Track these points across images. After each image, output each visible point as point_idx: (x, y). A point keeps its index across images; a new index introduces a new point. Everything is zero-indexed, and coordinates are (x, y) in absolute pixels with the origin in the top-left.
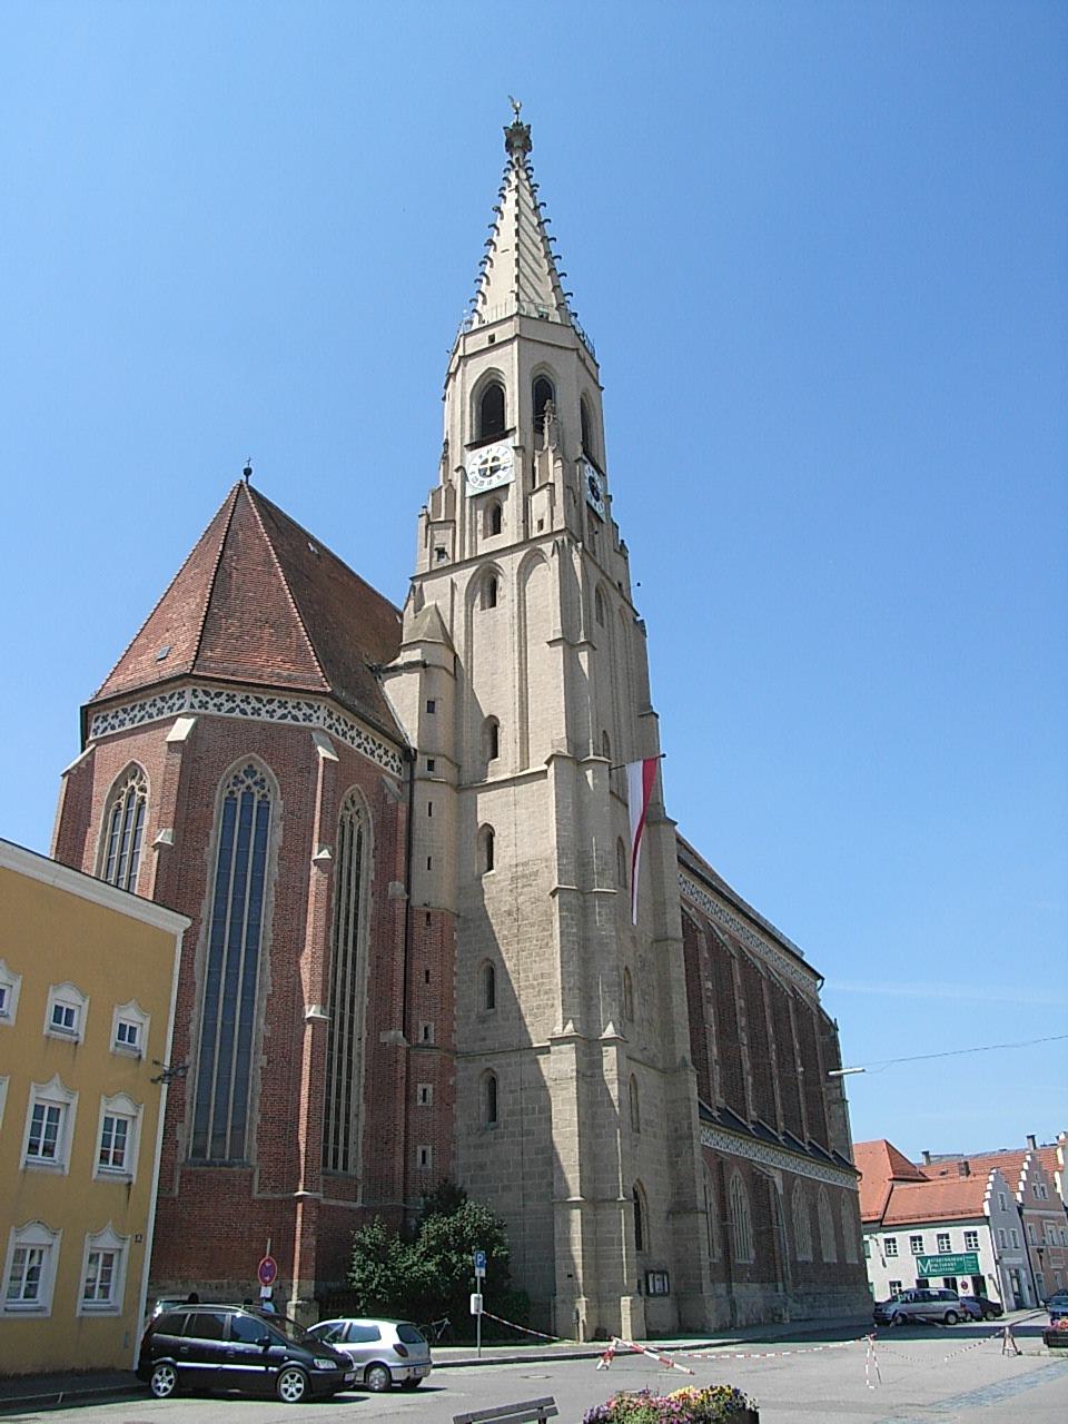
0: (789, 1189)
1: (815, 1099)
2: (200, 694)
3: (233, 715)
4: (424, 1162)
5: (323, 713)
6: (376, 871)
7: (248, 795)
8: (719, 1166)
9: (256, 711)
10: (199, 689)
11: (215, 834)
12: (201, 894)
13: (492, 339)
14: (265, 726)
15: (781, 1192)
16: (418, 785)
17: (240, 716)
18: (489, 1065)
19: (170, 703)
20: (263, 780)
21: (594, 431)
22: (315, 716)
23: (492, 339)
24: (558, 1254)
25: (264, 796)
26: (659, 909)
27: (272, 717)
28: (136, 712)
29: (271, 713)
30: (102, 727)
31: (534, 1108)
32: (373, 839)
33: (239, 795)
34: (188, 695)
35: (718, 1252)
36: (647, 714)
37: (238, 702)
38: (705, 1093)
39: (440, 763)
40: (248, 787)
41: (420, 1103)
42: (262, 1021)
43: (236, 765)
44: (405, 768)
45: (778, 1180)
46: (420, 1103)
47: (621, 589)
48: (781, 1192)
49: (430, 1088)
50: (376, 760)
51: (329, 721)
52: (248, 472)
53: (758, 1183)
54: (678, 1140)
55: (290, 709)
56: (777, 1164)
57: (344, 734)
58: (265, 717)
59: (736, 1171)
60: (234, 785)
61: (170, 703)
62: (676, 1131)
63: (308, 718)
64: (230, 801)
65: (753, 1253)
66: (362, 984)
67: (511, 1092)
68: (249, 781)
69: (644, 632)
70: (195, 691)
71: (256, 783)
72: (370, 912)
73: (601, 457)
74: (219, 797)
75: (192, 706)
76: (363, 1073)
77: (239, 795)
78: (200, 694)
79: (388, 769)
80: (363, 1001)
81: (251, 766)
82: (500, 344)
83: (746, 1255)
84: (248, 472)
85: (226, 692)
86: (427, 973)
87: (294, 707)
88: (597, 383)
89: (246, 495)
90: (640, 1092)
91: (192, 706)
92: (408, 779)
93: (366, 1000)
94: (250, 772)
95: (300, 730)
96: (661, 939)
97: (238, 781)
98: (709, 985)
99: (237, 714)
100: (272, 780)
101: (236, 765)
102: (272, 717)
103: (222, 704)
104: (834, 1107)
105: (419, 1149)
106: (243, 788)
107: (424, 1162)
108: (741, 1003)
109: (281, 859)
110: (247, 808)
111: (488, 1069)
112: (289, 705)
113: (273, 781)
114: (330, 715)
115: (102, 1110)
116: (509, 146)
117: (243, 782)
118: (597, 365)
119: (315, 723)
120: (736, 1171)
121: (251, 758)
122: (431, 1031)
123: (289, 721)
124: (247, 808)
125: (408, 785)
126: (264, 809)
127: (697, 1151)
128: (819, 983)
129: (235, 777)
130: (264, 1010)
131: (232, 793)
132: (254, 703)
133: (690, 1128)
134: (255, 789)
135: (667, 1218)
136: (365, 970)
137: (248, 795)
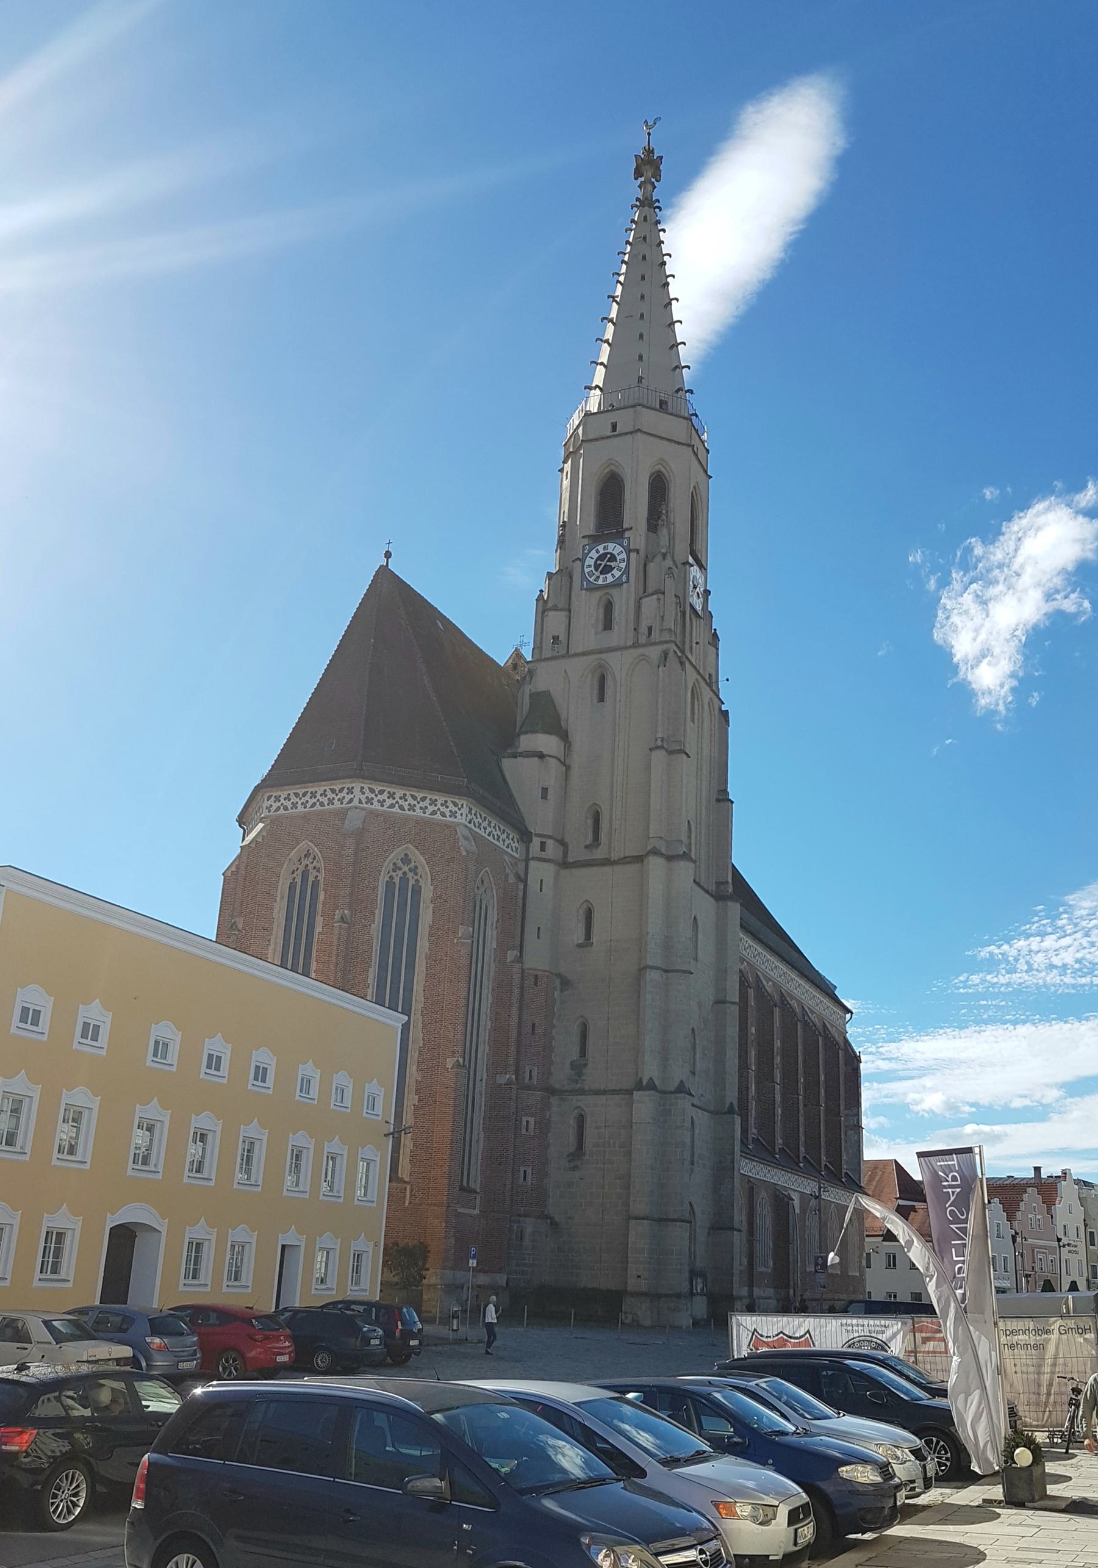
0: (803, 1210)
1: (834, 1128)
2: (367, 791)
3: (393, 810)
4: (525, 1179)
5: (465, 810)
6: (497, 940)
7: (404, 879)
8: (752, 1187)
9: (412, 808)
10: (366, 786)
11: (379, 913)
12: (369, 964)
13: (614, 427)
14: (419, 822)
15: (797, 1211)
16: (533, 864)
17: (298, 791)
18: (579, 1104)
19: (340, 796)
20: (416, 867)
21: (700, 523)
22: (459, 812)
23: (614, 427)
24: (630, 1260)
25: (417, 881)
26: (721, 973)
27: (382, 806)
28: (307, 798)
29: (382, 803)
30: (275, 805)
31: (614, 1143)
32: (496, 913)
33: (397, 880)
34: (357, 791)
35: (745, 1261)
36: (723, 798)
37: (397, 799)
38: (745, 1131)
39: (550, 843)
40: (405, 873)
41: (524, 1131)
42: (414, 1068)
43: (395, 855)
44: (521, 847)
45: (796, 1203)
46: (524, 1131)
47: (712, 682)
48: (797, 1211)
49: (532, 1120)
50: (500, 844)
51: (470, 817)
52: (388, 555)
53: (781, 1201)
54: (723, 1170)
55: (439, 806)
56: (798, 1186)
57: (479, 827)
58: (418, 813)
59: (763, 1194)
60: (394, 871)
61: (340, 796)
62: (721, 1162)
63: (453, 814)
64: (390, 884)
65: (771, 1263)
66: (484, 1036)
67: (597, 1128)
68: (406, 869)
69: (727, 722)
70: (362, 788)
71: (410, 870)
72: (492, 974)
73: (704, 554)
74: (383, 879)
75: (360, 802)
76: (483, 1108)
77: (397, 880)
78: (367, 791)
79: (509, 850)
80: (484, 1050)
81: (406, 855)
82: (620, 435)
83: (766, 1266)
84: (388, 555)
85: (388, 790)
86: (534, 1025)
87: (442, 805)
88: (706, 472)
89: (384, 575)
90: (697, 1131)
91: (360, 802)
92: (524, 857)
93: (487, 1048)
94: (406, 860)
95: (447, 826)
96: (720, 1002)
97: (396, 868)
98: (753, 1030)
99: (396, 809)
100: (424, 868)
101: (395, 855)
102: (382, 806)
103: (384, 801)
104: (850, 1132)
105: (522, 1169)
106: (400, 873)
107: (525, 1179)
108: (778, 1043)
109: (431, 935)
110: (403, 890)
111: (577, 1108)
112: (439, 803)
113: (425, 869)
114: (470, 812)
115: (18, 1000)
116: (638, 173)
117: (400, 869)
118: (708, 451)
119: (459, 819)
120: (763, 1194)
121: (407, 848)
122: (535, 1074)
123: (438, 816)
124: (403, 890)
125: (524, 864)
126: (417, 891)
127: (737, 1180)
128: (848, 1016)
129: (394, 864)
130: (416, 1059)
131: (391, 877)
132: (410, 800)
133: (733, 1162)
134: (410, 875)
135: (709, 1234)
136: (486, 1023)
137: (404, 879)
